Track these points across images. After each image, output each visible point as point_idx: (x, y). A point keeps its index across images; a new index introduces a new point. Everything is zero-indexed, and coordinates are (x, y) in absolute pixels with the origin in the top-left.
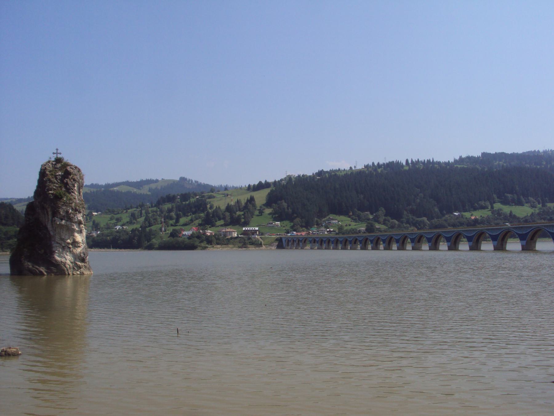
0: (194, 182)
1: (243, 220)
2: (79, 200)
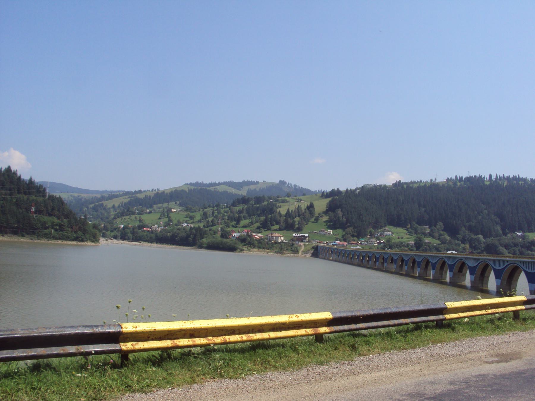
0: (293, 186)
1: (297, 226)
2: (33, 200)
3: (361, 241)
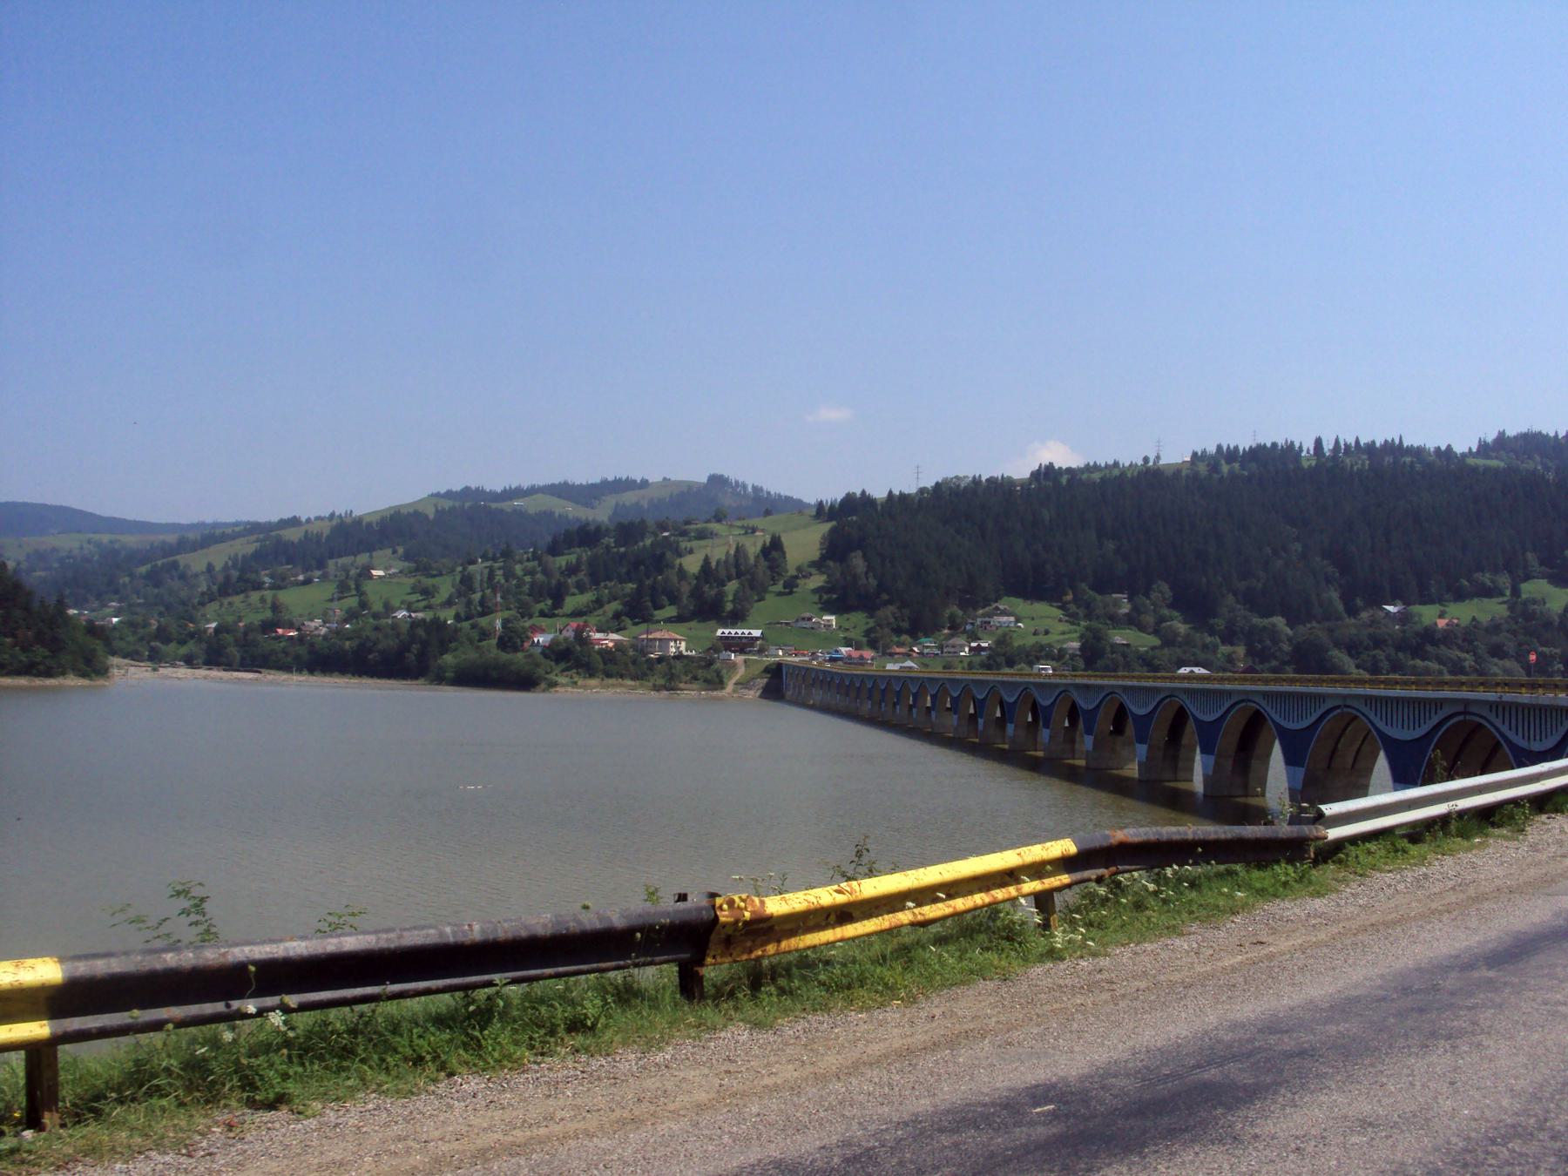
0: (750, 489)
1: (729, 607)
3: (921, 647)
